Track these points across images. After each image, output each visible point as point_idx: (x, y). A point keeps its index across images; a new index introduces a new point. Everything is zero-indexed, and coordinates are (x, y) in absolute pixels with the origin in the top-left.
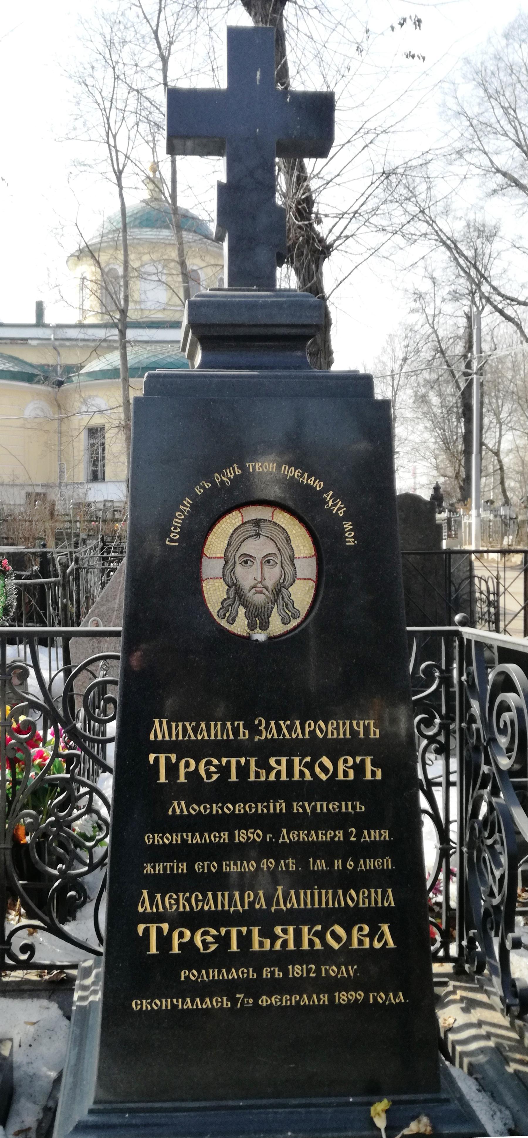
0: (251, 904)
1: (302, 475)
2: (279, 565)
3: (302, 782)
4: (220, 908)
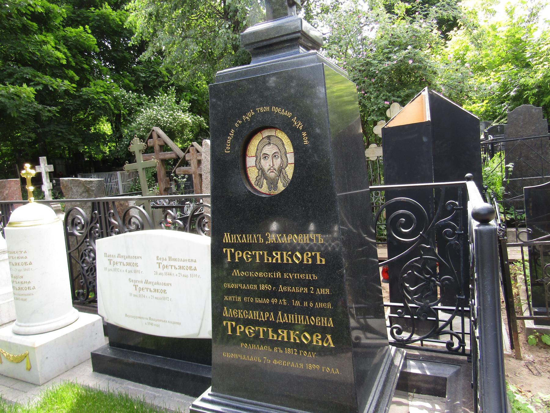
0: (268, 318)
1: (282, 110)
2: (280, 158)
3: (287, 264)
4: (255, 318)
